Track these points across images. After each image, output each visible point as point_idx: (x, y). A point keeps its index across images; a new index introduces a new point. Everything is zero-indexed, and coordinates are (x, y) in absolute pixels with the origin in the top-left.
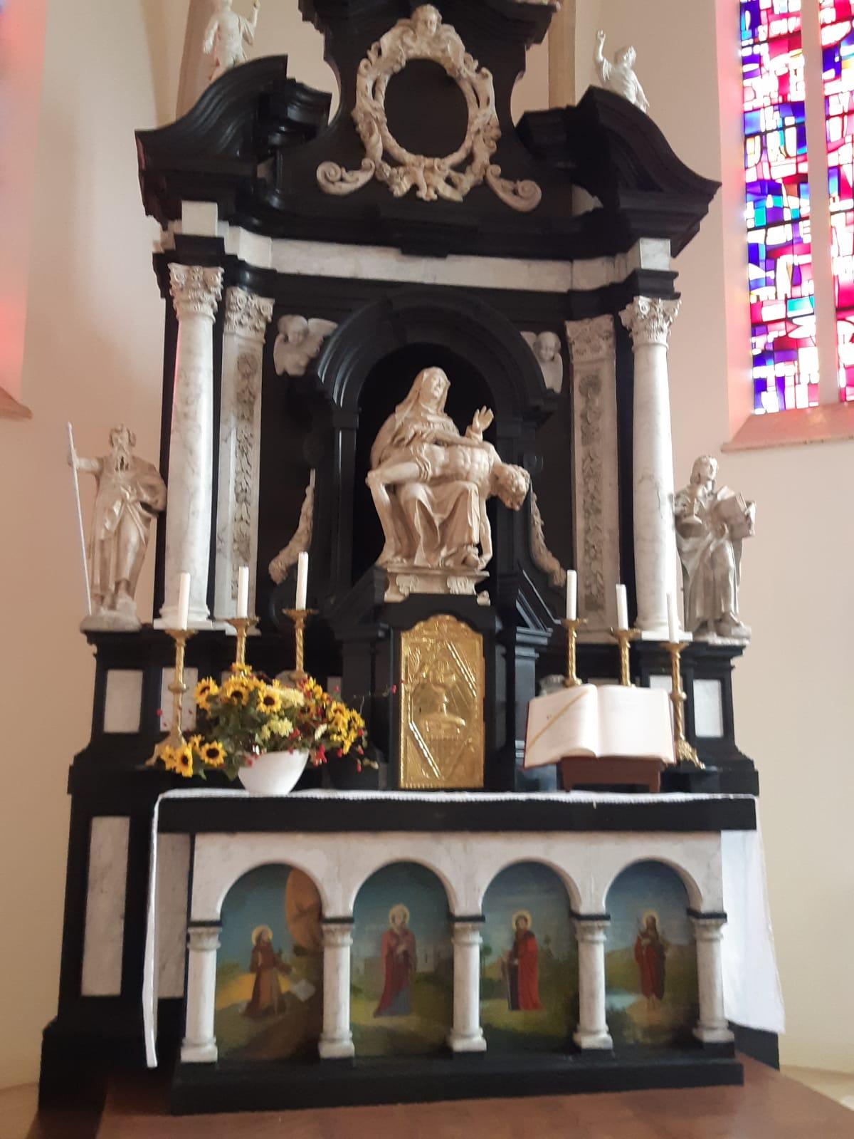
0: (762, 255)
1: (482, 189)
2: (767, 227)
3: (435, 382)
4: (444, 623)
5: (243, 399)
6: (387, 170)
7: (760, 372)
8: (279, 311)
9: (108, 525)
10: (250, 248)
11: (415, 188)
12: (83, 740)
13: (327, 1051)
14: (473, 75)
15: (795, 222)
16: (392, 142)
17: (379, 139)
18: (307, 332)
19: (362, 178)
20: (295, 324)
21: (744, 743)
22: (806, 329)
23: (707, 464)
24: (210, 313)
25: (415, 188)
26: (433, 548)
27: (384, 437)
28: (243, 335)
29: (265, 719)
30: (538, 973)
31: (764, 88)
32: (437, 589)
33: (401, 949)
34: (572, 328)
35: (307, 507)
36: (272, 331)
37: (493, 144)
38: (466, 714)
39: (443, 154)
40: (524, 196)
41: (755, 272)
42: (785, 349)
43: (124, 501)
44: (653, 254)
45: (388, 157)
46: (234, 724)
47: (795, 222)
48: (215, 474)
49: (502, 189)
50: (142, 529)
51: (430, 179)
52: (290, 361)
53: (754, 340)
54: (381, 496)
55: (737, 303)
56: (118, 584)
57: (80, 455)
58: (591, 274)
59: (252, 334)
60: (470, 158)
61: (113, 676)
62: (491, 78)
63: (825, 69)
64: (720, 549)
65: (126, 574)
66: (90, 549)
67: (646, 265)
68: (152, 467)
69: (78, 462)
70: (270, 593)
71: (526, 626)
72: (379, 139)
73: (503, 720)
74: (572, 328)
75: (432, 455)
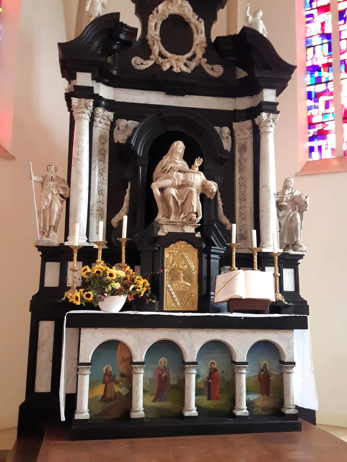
0: (313, 96)
1: (199, 68)
2: (315, 84)
3: (179, 146)
4: (182, 245)
5: (102, 153)
6: (160, 60)
7: (312, 144)
8: (116, 117)
9: (46, 203)
10: (104, 91)
11: (172, 67)
12: (36, 290)
13: (133, 415)
14: (196, 22)
15: (327, 82)
16: (163, 49)
17: (157, 47)
18: (127, 127)
19: (150, 63)
20: (122, 123)
21: (303, 294)
22: (331, 126)
23: (289, 181)
24: (88, 117)
25: (172, 67)
26: (178, 214)
27: (158, 169)
28: (101, 127)
29: (109, 282)
30: (219, 384)
31: (314, 28)
32: (179, 231)
33: (164, 375)
34: (235, 125)
35: (127, 197)
36: (113, 125)
37: (204, 50)
38: (190, 281)
39: (183, 54)
40: (216, 71)
41: (310, 103)
42: (322, 134)
43: (52, 194)
44: (269, 95)
45: (164, 57)
46: (97, 285)
47: (327, 82)
48: (90, 183)
49: (207, 68)
50: (60, 205)
51: (177, 64)
52: (120, 138)
53: (309, 130)
54: (157, 192)
55: (303, 115)
56: (50, 227)
57: (35, 175)
58: (243, 103)
59: (105, 126)
60: (194, 55)
61: (49, 265)
62: (203, 23)
63: (340, 20)
64: (294, 215)
65: (53, 223)
66: (39, 213)
67: (266, 99)
68: (64, 180)
69: (34, 178)
70: (112, 232)
71: (216, 246)
72: (157, 47)
73: (206, 284)
74: (235, 125)
75: (177, 176)
